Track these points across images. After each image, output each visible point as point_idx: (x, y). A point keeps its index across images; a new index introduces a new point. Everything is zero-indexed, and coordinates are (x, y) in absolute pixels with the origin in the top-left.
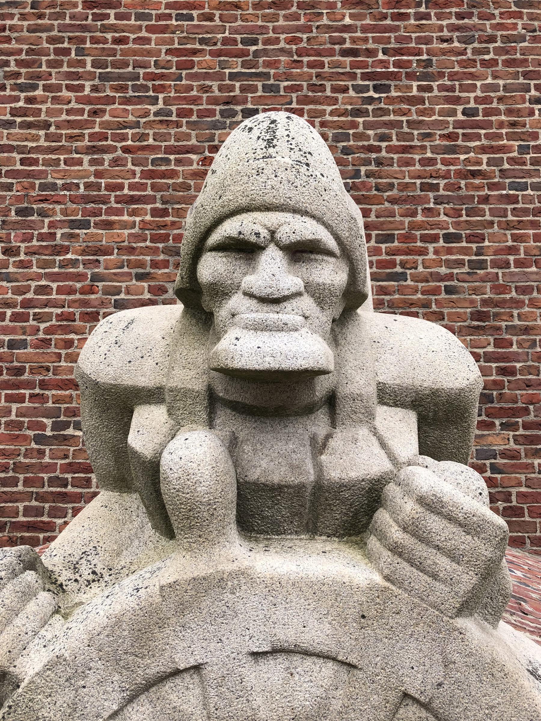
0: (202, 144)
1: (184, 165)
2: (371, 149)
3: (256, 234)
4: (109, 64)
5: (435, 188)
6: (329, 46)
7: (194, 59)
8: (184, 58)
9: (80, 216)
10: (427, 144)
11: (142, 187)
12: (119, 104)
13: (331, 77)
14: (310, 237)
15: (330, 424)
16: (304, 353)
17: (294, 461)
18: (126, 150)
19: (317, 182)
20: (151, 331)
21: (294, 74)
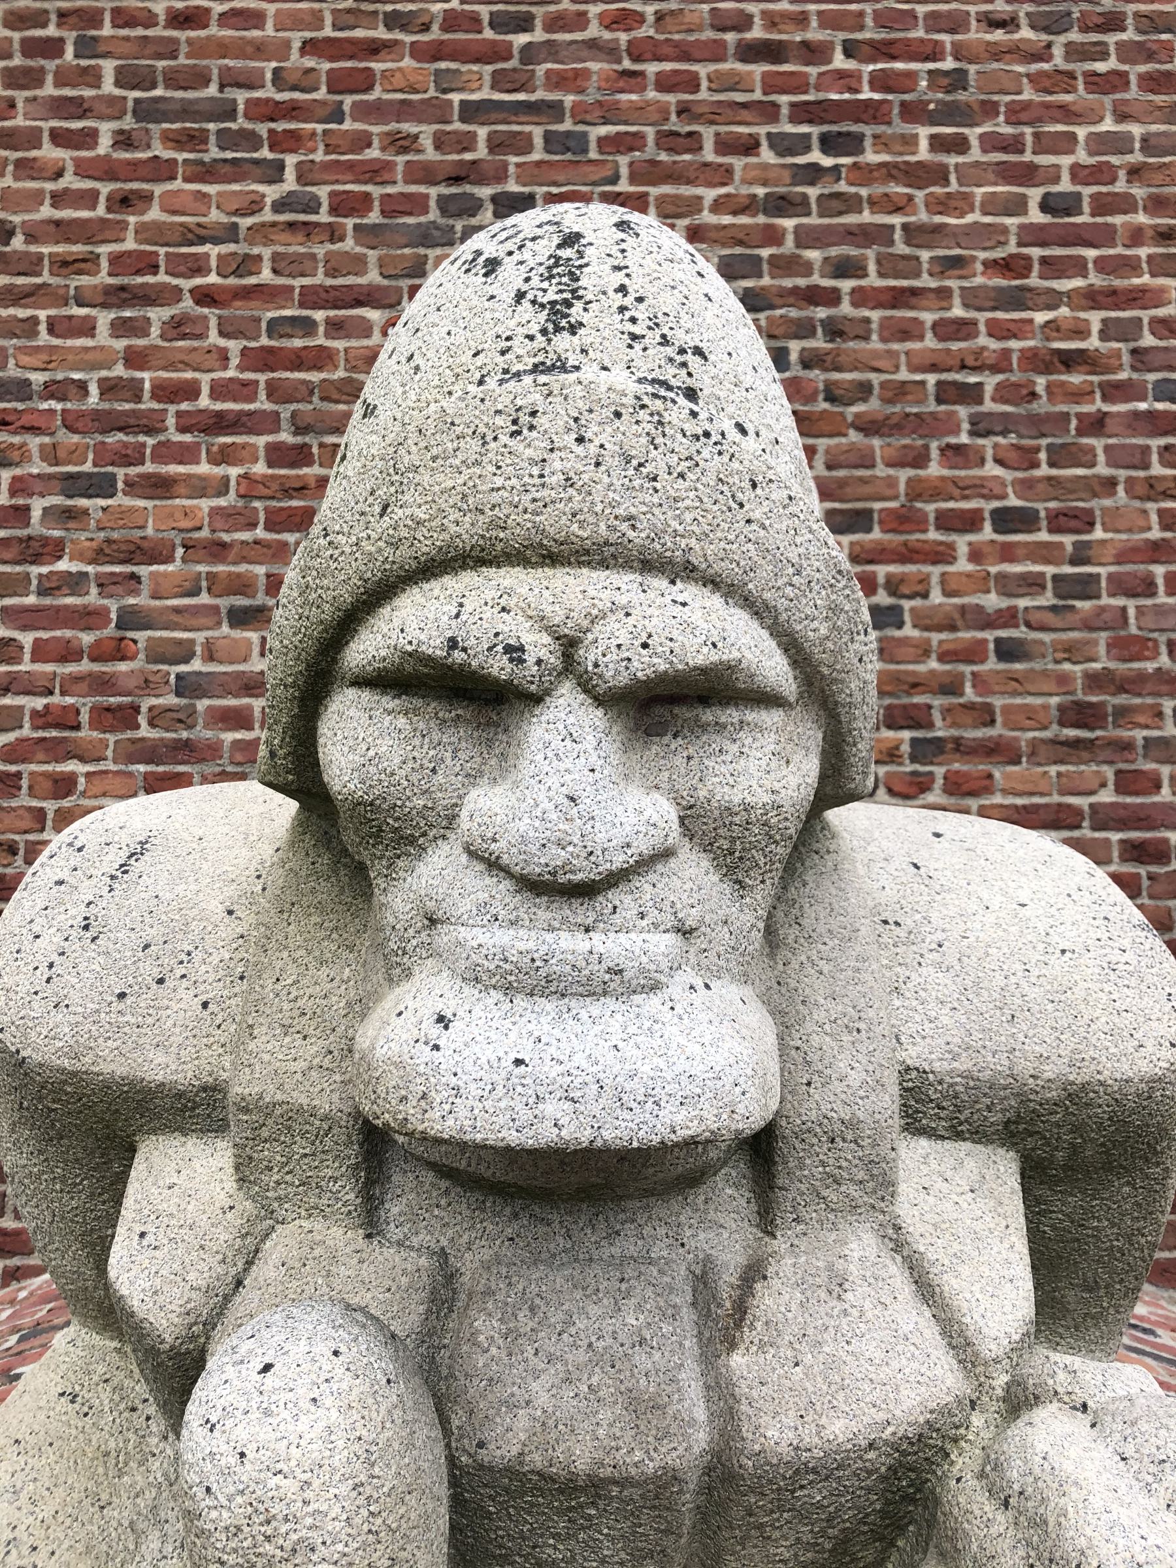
0: (393, 283)
1: (348, 337)
2: (814, 296)
3: (508, 649)
4: (160, 79)
5: (972, 394)
6: (709, 34)
7: (373, 65)
8: (349, 64)
9: (89, 464)
10: (953, 284)
11: (246, 390)
12: (186, 180)
13: (714, 115)
14: (703, 657)
15: (755, 1219)
16: (684, 1080)
17: (643, 1382)
18: (205, 297)
19: (726, 458)
20: (193, 887)
21: (623, 106)
